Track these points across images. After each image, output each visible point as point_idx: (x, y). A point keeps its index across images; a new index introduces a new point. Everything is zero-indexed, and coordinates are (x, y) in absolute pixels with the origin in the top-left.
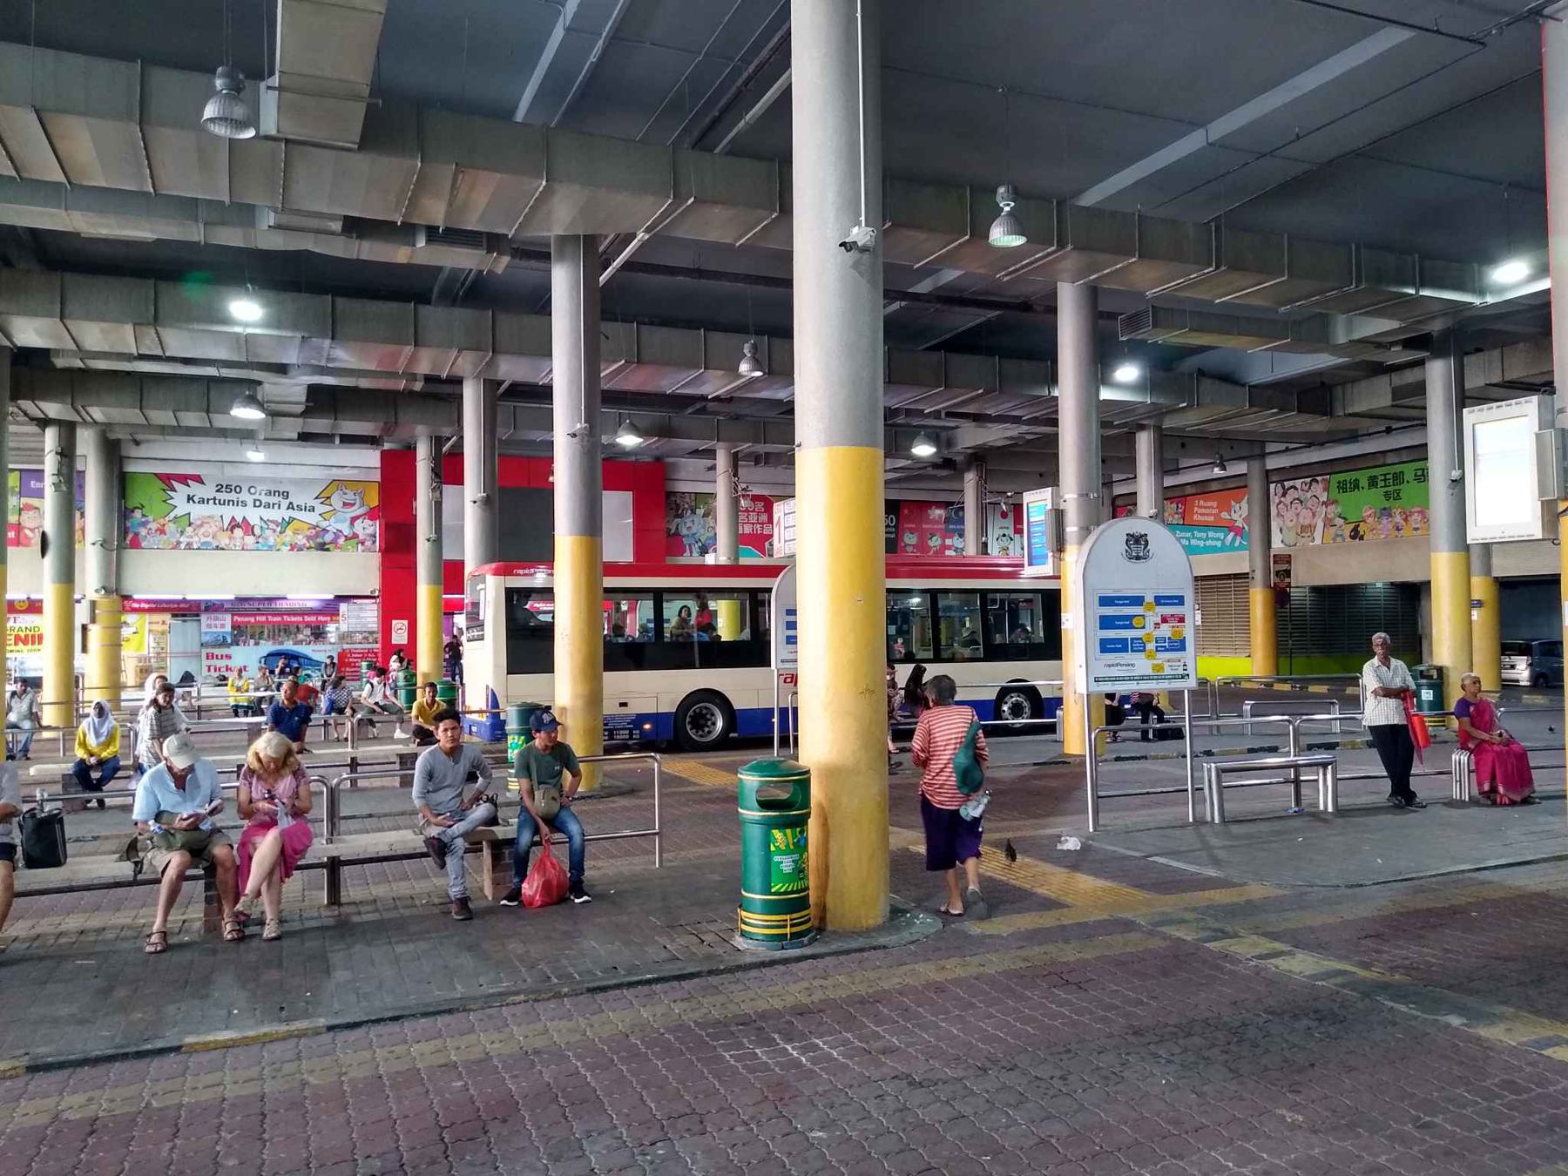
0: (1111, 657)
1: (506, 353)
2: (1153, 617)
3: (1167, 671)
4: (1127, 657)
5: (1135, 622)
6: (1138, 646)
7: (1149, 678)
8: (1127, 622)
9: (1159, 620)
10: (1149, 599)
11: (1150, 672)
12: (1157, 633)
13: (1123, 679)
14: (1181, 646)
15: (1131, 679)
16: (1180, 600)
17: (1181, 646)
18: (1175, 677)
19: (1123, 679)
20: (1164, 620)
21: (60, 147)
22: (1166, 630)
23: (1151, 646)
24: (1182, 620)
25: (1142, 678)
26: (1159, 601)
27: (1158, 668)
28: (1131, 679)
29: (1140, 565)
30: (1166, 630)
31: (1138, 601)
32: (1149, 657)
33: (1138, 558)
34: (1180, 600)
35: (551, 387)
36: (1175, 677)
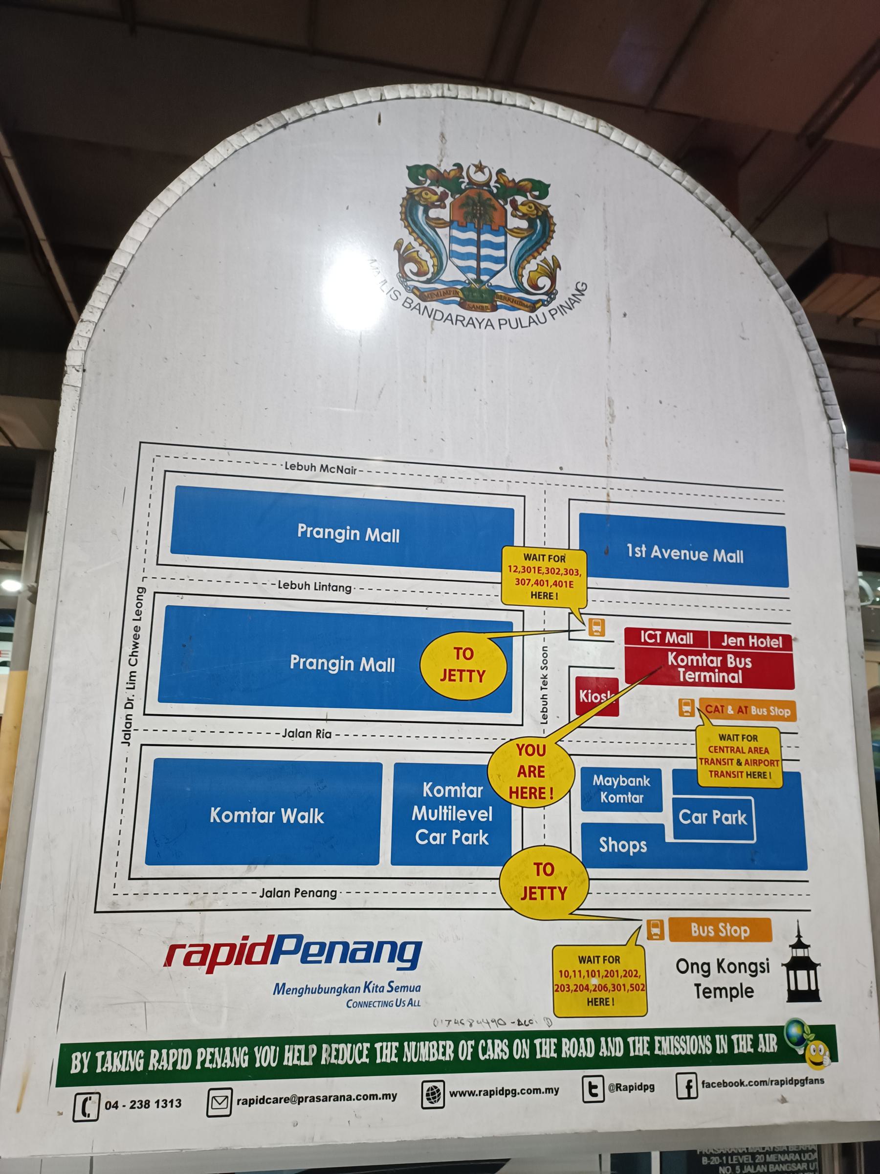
0: (233, 898)
1: (845, 270)
2: (567, 641)
3: (671, 1002)
4: (372, 897)
5: (435, 661)
6: (458, 823)
7: (525, 1052)
8: (387, 664)
9: (608, 658)
10: (547, 526)
11: (539, 1009)
12: (601, 744)
13: (315, 1059)
14: (773, 832)
15: (377, 1058)
16: (760, 555)
17: (773, 832)
18: (726, 1049)
19: (315, 1059)
20: (649, 660)
21: (26, 829)
22: (659, 727)
23: (548, 827)
24: (772, 666)
25: (471, 1053)
26: (612, 544)
27: (596, 976)
28: (377, 1058)
29: (499, 338)
30: (659, 727)
31: (470, 537)
32: (538, 894)
33: (479, 297)
34: (760, 555)
35: (844, 1145)
36: (726, 1049)
